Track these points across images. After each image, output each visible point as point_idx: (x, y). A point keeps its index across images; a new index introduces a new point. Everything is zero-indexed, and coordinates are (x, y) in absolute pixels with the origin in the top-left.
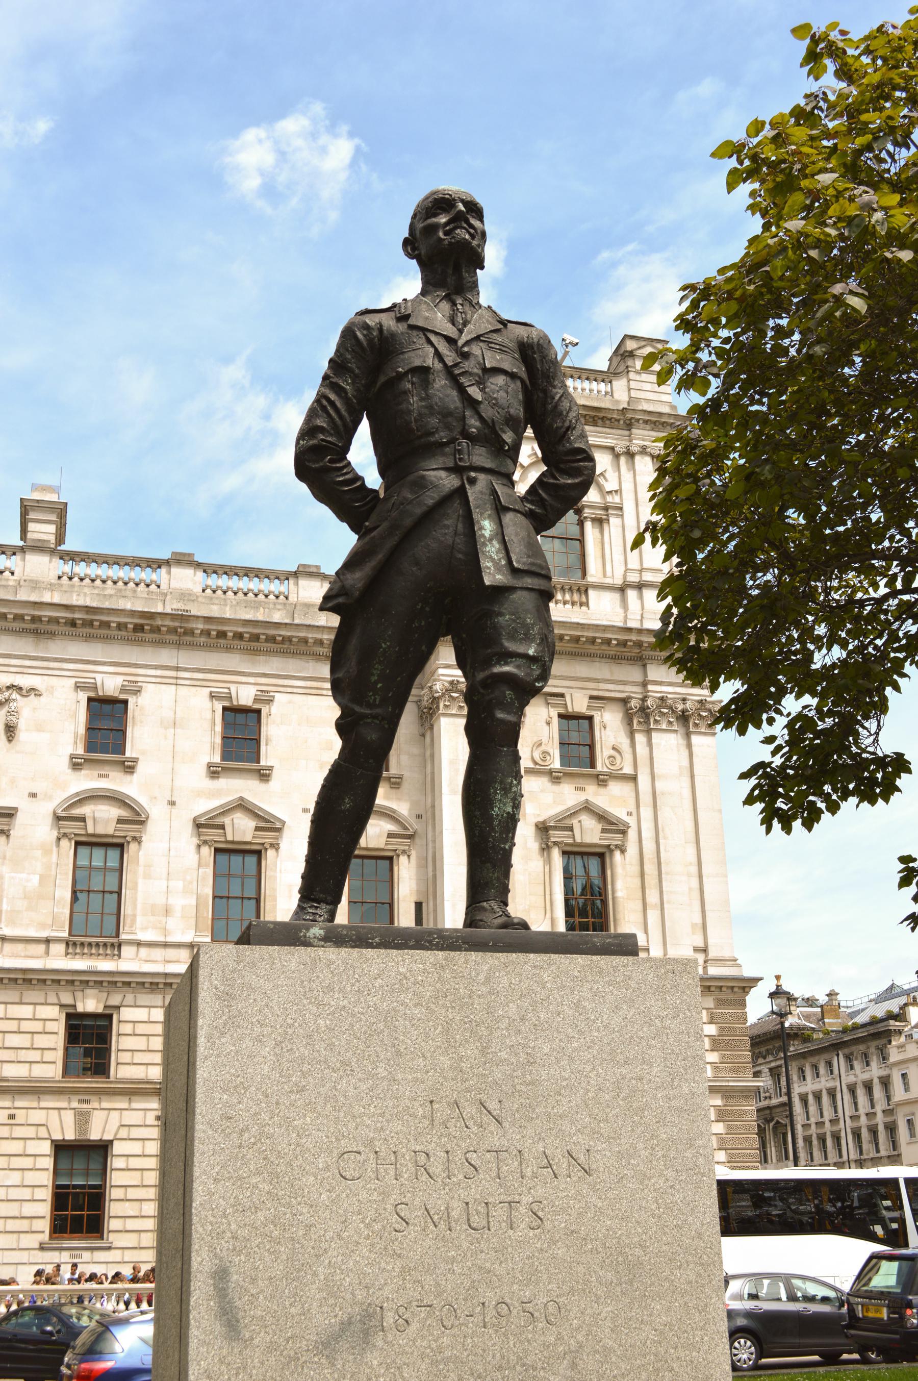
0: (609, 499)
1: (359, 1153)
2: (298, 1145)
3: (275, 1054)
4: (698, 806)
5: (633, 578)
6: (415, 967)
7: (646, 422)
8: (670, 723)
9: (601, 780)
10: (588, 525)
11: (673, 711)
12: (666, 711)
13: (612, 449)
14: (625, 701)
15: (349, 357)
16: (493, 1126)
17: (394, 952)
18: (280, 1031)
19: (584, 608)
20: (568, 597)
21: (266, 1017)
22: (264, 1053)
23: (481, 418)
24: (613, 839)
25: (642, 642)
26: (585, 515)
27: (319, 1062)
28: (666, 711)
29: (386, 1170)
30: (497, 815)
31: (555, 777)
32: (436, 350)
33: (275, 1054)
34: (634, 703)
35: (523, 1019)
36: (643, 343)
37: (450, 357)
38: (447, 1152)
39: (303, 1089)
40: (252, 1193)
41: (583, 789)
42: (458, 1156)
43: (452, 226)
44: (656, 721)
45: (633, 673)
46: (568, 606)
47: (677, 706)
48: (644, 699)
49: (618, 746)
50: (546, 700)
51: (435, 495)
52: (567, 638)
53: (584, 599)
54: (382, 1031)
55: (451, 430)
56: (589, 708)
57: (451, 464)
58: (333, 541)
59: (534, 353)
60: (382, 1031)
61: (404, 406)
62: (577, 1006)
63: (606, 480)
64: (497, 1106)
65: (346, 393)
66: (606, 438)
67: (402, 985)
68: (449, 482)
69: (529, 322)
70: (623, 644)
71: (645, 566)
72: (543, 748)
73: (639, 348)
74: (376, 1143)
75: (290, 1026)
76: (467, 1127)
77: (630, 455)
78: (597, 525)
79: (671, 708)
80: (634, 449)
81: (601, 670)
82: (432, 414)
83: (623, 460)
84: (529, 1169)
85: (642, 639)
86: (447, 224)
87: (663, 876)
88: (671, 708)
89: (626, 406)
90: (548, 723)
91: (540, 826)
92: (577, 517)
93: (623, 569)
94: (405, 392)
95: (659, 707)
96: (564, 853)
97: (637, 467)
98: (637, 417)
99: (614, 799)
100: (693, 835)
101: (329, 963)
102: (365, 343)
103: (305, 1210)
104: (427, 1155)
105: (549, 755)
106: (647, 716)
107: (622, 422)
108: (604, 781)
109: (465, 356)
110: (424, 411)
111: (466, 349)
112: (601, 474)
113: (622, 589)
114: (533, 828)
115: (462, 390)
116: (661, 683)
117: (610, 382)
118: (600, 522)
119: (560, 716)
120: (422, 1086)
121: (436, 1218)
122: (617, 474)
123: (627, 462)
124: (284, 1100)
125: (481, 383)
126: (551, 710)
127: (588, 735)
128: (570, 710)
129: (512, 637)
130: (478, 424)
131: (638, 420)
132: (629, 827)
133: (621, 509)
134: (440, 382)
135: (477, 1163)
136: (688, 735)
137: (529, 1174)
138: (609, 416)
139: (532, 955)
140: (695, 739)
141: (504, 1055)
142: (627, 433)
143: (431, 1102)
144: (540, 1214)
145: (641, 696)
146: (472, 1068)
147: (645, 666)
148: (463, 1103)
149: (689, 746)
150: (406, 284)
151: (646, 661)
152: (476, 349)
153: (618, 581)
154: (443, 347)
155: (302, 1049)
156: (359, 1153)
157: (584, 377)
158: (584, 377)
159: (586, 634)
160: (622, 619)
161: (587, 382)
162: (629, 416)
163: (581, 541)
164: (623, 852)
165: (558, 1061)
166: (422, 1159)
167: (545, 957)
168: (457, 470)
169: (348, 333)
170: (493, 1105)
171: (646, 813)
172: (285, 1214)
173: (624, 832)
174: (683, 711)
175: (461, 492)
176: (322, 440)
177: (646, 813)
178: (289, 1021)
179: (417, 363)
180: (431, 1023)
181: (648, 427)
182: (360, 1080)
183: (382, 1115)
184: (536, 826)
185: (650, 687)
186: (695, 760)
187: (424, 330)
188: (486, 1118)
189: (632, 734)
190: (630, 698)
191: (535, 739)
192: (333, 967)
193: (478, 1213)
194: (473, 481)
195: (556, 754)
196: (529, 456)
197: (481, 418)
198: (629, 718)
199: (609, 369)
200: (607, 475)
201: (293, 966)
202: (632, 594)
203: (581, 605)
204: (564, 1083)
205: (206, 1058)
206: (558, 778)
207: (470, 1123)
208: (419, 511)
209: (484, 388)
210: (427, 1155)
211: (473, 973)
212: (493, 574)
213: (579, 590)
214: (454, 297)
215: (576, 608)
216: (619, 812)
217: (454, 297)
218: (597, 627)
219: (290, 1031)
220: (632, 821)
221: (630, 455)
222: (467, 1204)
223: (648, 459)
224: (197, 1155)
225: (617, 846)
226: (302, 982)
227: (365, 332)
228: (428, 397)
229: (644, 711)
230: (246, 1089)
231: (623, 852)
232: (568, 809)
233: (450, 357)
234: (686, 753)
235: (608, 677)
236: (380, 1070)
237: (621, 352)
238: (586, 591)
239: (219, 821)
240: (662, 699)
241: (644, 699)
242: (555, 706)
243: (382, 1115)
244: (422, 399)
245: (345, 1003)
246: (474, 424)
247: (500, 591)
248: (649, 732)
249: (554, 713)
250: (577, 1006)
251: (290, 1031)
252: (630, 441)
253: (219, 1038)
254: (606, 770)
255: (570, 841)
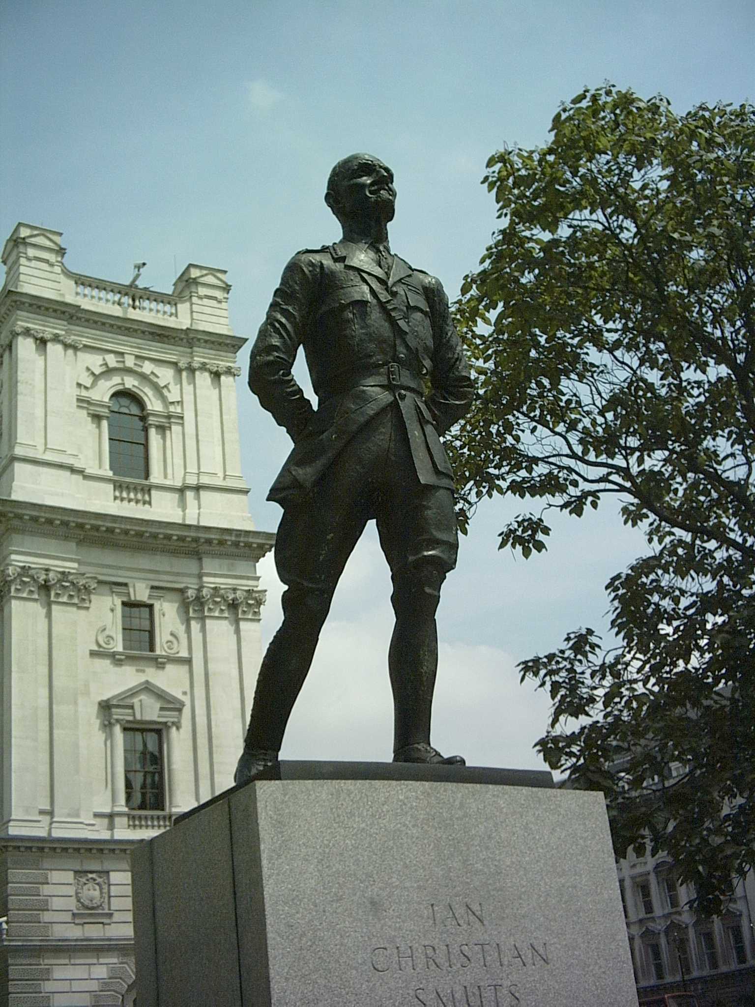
0: (172, 409)
1: (385, 949)
2: (342, 945)
3: (318, 870)
4: (245, 685)
5: (192, 481)
6: (409, 794)
7: (206, 341)
8: (222, 610)
9: (159, 663)
10: (152, 432)
11: (225, 600)
12: (218, 599)
13: (175, 364)
14: (182, 591)
15: (297, 288)
16: (478, 924)
17: (394, 783)
18: (320, 851)
19: (147, 506)
20: (132, 495)
21: (309, 840)
22: (310, 870)
23: (407, 346)
24: (169, 717)
25: (199, 538)
26: (150, 422)
27: (350, 876)
28: (218, 599)
29: (406, 962)
30: (426, 672)
31: (116, 659)
32: (371, 288)
33: (318, 870)
34: (191, 593)
35: (490, 837)
36: (205, 272)
37: (384, 296)
38: (447, 946)
39: (341, 899)
40: (314, 987)
41: (143, 671)
42: (455, 950)
43: (376, 187)
44: (210, 609)
45: (190, 565)
46: (133, 504)
47: (229, 595)
48: (199, 590)
49: (176, 632)
50: (111, 589)
51: (375, 407)
52: (132, 533)
53: (147, 498)
54: (392, 848)
55: (386, 354)
56: (150, 597)
57: (386, 383)
58: (279, 445)
59: (434, 296)
60: (392, 848)
61: (348, 332)
62: (526, 828)
63: (169, 391)
64: (479, 908)
65: (295, 318)
66: (171, 354)
67: (402, 810)
68: (385, 397)
69: (424, 270)
70: (182, 539)
71: (202, 470)
72: (107, 633)
73: (202, 276)
74: (398, 940)
75: (327, 846)
76: (459, 925)
77: (192, 370)
78: (160, 431)
79: (222, 597)
80: (196, 365)
81: (162, 563)
82: (370, 341)
83: (184, 374)
84: (506, 959)
85: (200, 535)
86: (372, 184)
87: (214, 749)
88: (222, 597)
89: (189, 326)
90: (112, 610)
91: (104, 704)
92: (142, 424)
93: (183, 472)
94: (348, 321)
95: (213, 596)
96: (125, 729)
97: (197, 382)
98: (199, 337)
99: (171, 680)
100: (240, 711)
101: (349, 793)
102: (310, 277)
103: (352, 999)
104: (434, 948)
105: (113, 639)
106: (202, 604)
107: (185, 341)
108: (164, 663)
109: (394, 294)
110: (363, 337)
111: (394, 289)
112: (165, 386)
113: (182, 491)
114: (96, 707)
115: (393, 322)
116: (215, 575)
117: (176, 304)
118: (162, 429)
119: (124, 604)
120: (425, 892)
121: (444, 999)
122: (178, 386)
123: (187, 377)
124: (328, 908)
125: (406, 317)
126: (115, 598)
127: (148, 623)
128: (133, 598)
129: (439, 529)
130: (405, 351)
131: (199, 340)
132: (184, 706)
133: (182, 418)
134: (375, 315)
135: (469, 954)
136: (237, 621)
137: (506, 963)
138: (175, 335)
139: (490, 786)
140: (243, 625)
141: (479, 866)
142: (189, 350)
143: (432, 905)
144: (517, 995)
145: (196, 587)
146: (458, 877)
147: (200, 559)
148: (455, 906)
149: (238, 631)
150: (329, 230)
151: (203, 555)
152: (400, 289)
153: (178, 484)
154: (375, 285)
155: (337, 865)
156: (385, 949)
157: (152, 298)
158: (152, 298)
159: (150, 530)
160: (181, 517)
161: (155, 303)
162: (191, 336)
163: (146, 446)
164: (178, 728)
165: (517, 871)
166: (430, 951)
167: (500, 787)
168: (389, 387)
169: (293, 269)
170: (475, 907)
171: (199, 691)
172: (338, 1003)
173: (180, 710)
174: (233, 600)
175: (394, 407)
176: (277, 357)
177: (199, 691)
178: (326, 842)
179: (357, 297)
180: (426, 841)
181: (208, 346)
182: (380, 889)
183: (399, 917)
184: (100, 704)
185: (205, 579)
186: (243, 644)
187: (359, 271)
188: (472, 918)
189: (187, 622)
190: (187, 588)
191: (101, 624)
192: (352, 795)
193: (474, 994)
194: (403, 397)
195: (119, 637)
196: (101, 365)
197: (407, 346)
198: (185, 605)
199: (174, 292)
200: (170, 387)
201: (324, 796)
202: (190, 495)
203: (144, 503)
204: (523, 890)
205: (269, 876)
206: (121, 660)
207: (461, 922)
208: (362, 420)
209: (408, 322)
210: (434, 948)
211: (451, 800)
212: (425, 477)
213: (142, 490)
214: (377, 245)
215: (140, 505)
216: (176, 693)
217: (377, 245)
218: (160, 523)
219: (327, 850)
220: (186, 700)
221: (192, 370)
222: (465, 987)
223: (207, 374)
224: (270, 959)
225: (173, 723)
226: (332, 809)
227: (311, 269)
228: (368, 326)
229: (199, 601)
230: (301, 901)
231: (178, 728)
232: (130, 689)
233: (384, 296)
234: (234, 638)
235: (169, 569)
236: (394, 880)
237: (185, 278)
238: (149, 490)
239: (128, 702)
240: (215, 589)
241: (199, 590)
242: (119, 594)
243: (399, 917)
244: (362, 328)
245: (363, 825)
246: (402, 354)
247: (430, 488)
248: (202, 619)
249: (118, 602)
250: (526, 828)
251: (327, 850)
252: (192, 358)
253: (277, 859)
254: (164, 653)
255: (131, 718)
